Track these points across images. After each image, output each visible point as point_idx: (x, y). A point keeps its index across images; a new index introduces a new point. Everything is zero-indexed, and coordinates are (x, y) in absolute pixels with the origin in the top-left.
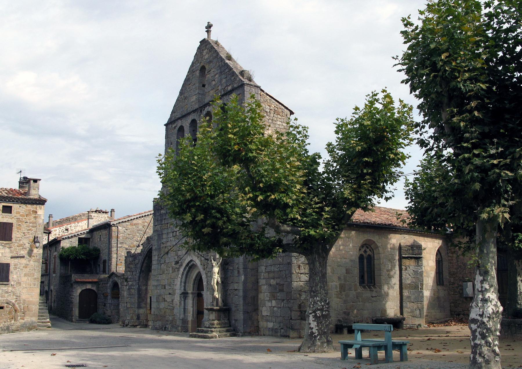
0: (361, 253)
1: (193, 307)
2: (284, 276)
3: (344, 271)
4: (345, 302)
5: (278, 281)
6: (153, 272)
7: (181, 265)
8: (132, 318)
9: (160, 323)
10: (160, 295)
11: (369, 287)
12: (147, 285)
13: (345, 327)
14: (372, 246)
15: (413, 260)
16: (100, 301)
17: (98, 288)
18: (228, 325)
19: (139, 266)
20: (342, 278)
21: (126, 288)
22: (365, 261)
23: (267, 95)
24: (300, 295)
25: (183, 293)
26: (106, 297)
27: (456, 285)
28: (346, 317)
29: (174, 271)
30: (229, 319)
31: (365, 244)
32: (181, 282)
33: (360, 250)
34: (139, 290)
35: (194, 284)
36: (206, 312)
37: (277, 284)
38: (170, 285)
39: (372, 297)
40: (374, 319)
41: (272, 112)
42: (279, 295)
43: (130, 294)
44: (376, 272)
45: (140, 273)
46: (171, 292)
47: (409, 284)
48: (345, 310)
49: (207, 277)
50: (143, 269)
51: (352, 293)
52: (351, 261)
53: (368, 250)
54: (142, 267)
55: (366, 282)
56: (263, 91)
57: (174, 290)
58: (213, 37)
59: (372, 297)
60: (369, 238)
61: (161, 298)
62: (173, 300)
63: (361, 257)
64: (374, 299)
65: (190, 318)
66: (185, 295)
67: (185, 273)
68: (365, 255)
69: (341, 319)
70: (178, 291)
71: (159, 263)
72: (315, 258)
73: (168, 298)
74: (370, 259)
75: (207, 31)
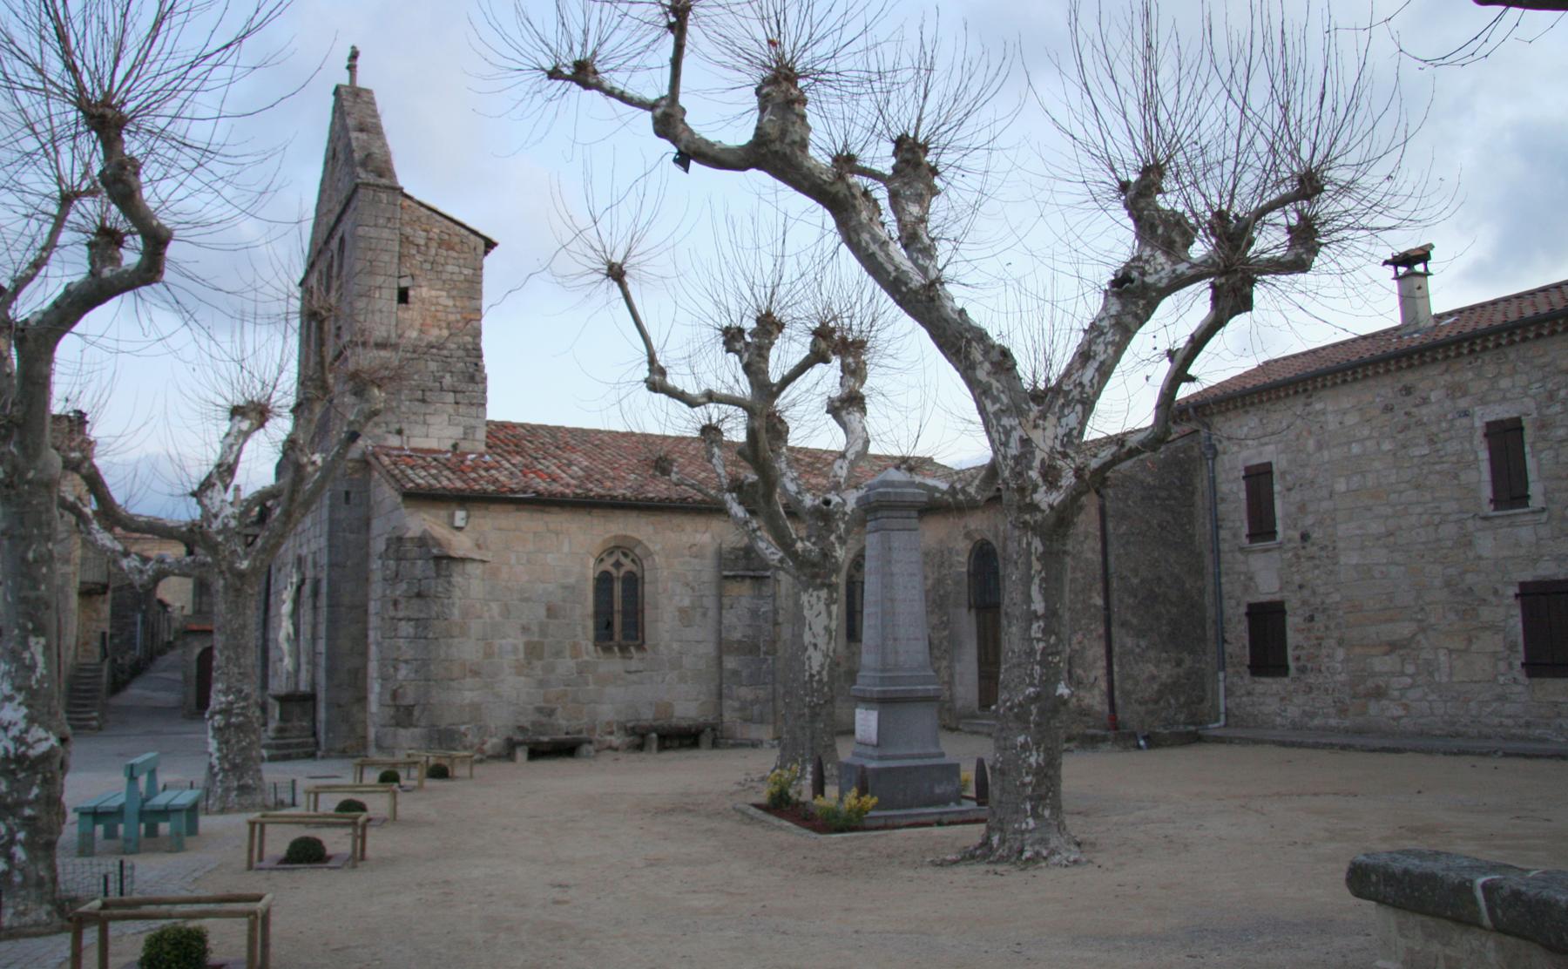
0: (602, 567)
3: (542, 612)
4: (542, 683)
13: (520, 744)
15: (748, 582)
23: (421, 204)
24: (396, 669)
31: (617, 547)
40: (630, 725)
41: (434, 245)
44: (647, 613)
47: (739, 642)
51: (566, 665)
52: (565, 587)
55: (617, 637)
56: (410, 198)
58: (361, 82)
63: (603, 582)
64: (634, 677)
75: (349, 68)
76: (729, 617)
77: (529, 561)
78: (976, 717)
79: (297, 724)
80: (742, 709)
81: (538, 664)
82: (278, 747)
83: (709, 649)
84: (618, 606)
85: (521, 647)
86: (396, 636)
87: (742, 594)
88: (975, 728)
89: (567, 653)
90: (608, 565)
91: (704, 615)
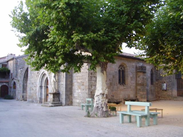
1: (45, 92)
2: (84, 78)
5: (82, 80)
6: (29, 77)
7: (40, 74)
8: (20, 97)
9: (31, 99)
10: (31, 87)
11: (123, 85)
12: (26, 83)
14: (124, 66)
16: (9, 90)
17: (8, 84)
18: (59, 101)
19: (23, 75)
20: (111, 80)
21: (18, 84)
22: (121, 72)
25: (40, 86)
26: (11, 87)
27: (159, 85)
28: (112, 98)
29: (37, 77)
30: (59, 98)
31: (122, 65)
32: (39, 81)
33: (119, 67)
34: (23, 85)
35: (45, 82)
36: (49, 94)
37: (81, 82)
38: (35, 83)
39: (124, 89)
40: (125, 99)
42: (82, 87)
43: (20, 87)
45: (24, 78)
46: (35, 86)
47: (140, 83)
48: (112, 95)
49: (50, 78)
50: (25, 76)
52: (115, 72)
53: (122, 68)
54: (24, 75)
55: (121, 82)
57: (37, 85)
59: (124, 89)
60: (123, 62)
61: (31, 88)
62: (36, 90)
63: (119, 71)
64: (125, 90)
65: (43, 97)
66: (41, 87)
67: (41, 77)
68: (121, 70)
69: (110, 99)
70: (38, 86)
71: (31, 74)
72: (88, 51)
73: (34, 89)
74: (123, 72)
76: (138, 79)
77: (110, 67)
78: (177, 98)
79: (56, 99)
80: (141, 96)
81: (111, 87)
82: (54, 104)
83: (134, 85)
84: (121, 76)
85: (109, 83)
86: (91, 80)
87: (141, 75)
88: (177, 99)
89: (116, 85)
90: (120, 69)
91: (134, 78)
